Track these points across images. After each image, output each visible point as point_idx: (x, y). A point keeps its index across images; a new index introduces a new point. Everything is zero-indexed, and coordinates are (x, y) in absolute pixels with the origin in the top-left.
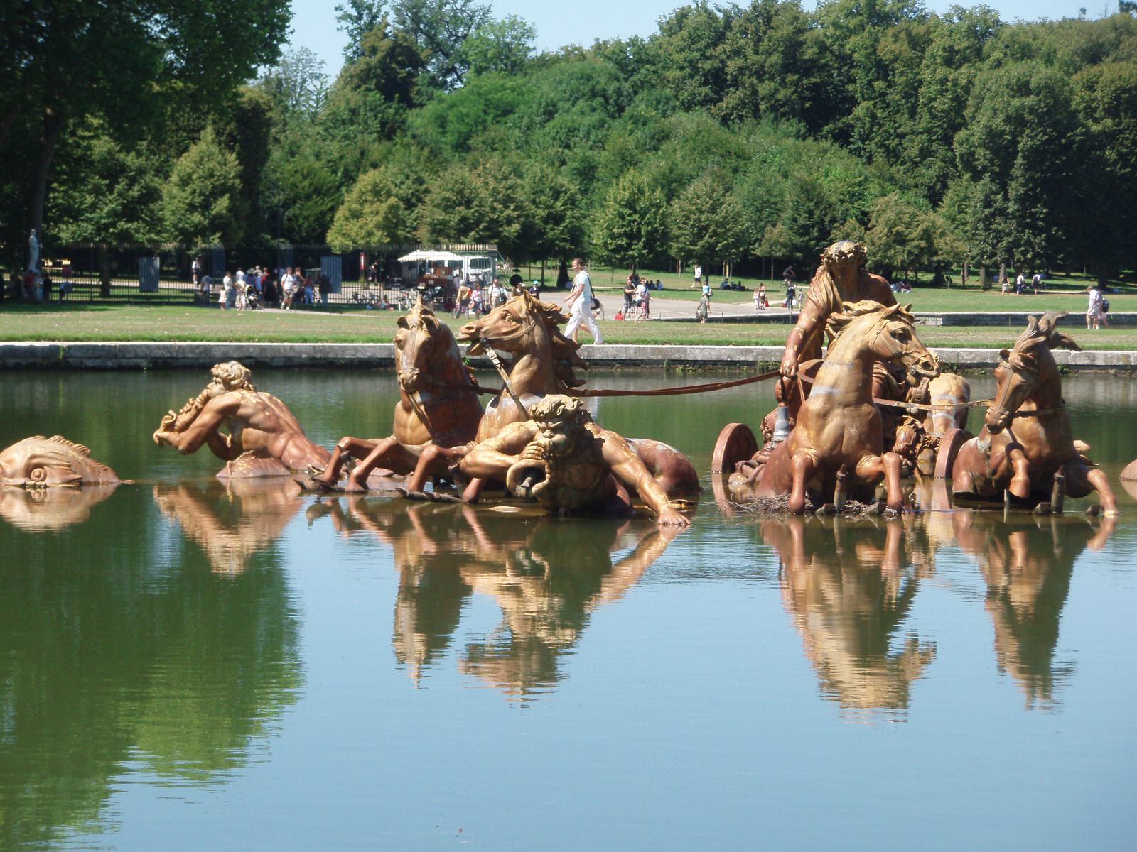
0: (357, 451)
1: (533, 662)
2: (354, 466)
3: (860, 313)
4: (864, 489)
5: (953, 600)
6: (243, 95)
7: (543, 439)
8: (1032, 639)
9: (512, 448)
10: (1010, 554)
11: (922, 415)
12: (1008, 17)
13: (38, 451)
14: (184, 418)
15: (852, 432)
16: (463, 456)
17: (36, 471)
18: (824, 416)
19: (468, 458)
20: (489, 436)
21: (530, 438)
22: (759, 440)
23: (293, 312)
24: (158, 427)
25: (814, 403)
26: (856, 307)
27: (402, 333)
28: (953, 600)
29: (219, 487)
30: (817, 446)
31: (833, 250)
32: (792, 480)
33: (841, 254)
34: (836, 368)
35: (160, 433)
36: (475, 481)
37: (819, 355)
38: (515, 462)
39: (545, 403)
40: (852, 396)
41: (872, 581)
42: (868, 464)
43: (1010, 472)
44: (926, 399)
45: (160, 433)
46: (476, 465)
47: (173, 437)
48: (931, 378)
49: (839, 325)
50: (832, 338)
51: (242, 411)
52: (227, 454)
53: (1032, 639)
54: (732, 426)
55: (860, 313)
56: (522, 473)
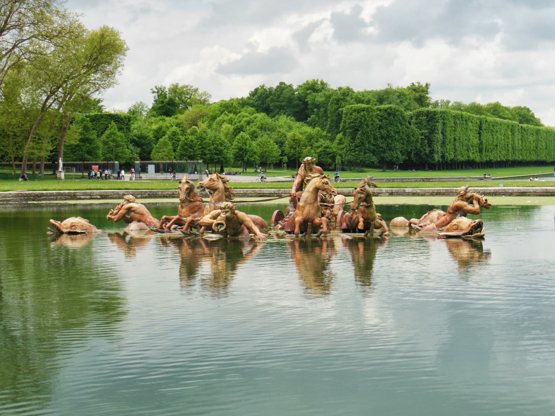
0: (168, 220)
1: (220, 283)
2: (166, 224)
3: (314, 177)
4: (316, 228)
5: (341, 266)
6: (439, 161)
7: (223, 215)
8: (364, 271)
9: (215, 218)
10: (358, 249)
11: (332, 207)
12: (356, 90)
13: (73, 221)
14: (115, 211)
15: (312, 211)
16: (199, 220)
17: (73, 227)
18: (304, 207)
19: (201, 221)
20: (207, 214)
21: (219, 214)
22: (285, 215)
23: (160, 176)
24: (108, 214)
25: (301, 204)
26: (313, 176)
27: (180, 186)
28: (341, 266)
29: (126, 234)
30: (302, 215)
31: (305, 159)
32: (295, 226)
33: (308, 161)
34: (306, 194)
35: (109, 216)
36: (203, 227)
37: (302, 190)
38: (215, 222)
39: (223, 204)
40: (312, 201)
41: (318, 259)
42: (317, 220)
43: (358, 222)
44: (333, 202)
45: (109, 216)
46: (203, 223)
47: (113, 217)
48: (335, 196)
49: (308, 181)
50: (306, 185)
51: (132, 209)
52: (129, 221)
53: (364, 271)
54: (277, 211)
55: (314, 177)
56: (218, 224)
